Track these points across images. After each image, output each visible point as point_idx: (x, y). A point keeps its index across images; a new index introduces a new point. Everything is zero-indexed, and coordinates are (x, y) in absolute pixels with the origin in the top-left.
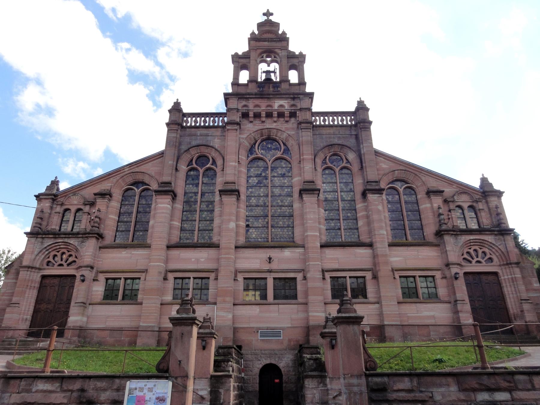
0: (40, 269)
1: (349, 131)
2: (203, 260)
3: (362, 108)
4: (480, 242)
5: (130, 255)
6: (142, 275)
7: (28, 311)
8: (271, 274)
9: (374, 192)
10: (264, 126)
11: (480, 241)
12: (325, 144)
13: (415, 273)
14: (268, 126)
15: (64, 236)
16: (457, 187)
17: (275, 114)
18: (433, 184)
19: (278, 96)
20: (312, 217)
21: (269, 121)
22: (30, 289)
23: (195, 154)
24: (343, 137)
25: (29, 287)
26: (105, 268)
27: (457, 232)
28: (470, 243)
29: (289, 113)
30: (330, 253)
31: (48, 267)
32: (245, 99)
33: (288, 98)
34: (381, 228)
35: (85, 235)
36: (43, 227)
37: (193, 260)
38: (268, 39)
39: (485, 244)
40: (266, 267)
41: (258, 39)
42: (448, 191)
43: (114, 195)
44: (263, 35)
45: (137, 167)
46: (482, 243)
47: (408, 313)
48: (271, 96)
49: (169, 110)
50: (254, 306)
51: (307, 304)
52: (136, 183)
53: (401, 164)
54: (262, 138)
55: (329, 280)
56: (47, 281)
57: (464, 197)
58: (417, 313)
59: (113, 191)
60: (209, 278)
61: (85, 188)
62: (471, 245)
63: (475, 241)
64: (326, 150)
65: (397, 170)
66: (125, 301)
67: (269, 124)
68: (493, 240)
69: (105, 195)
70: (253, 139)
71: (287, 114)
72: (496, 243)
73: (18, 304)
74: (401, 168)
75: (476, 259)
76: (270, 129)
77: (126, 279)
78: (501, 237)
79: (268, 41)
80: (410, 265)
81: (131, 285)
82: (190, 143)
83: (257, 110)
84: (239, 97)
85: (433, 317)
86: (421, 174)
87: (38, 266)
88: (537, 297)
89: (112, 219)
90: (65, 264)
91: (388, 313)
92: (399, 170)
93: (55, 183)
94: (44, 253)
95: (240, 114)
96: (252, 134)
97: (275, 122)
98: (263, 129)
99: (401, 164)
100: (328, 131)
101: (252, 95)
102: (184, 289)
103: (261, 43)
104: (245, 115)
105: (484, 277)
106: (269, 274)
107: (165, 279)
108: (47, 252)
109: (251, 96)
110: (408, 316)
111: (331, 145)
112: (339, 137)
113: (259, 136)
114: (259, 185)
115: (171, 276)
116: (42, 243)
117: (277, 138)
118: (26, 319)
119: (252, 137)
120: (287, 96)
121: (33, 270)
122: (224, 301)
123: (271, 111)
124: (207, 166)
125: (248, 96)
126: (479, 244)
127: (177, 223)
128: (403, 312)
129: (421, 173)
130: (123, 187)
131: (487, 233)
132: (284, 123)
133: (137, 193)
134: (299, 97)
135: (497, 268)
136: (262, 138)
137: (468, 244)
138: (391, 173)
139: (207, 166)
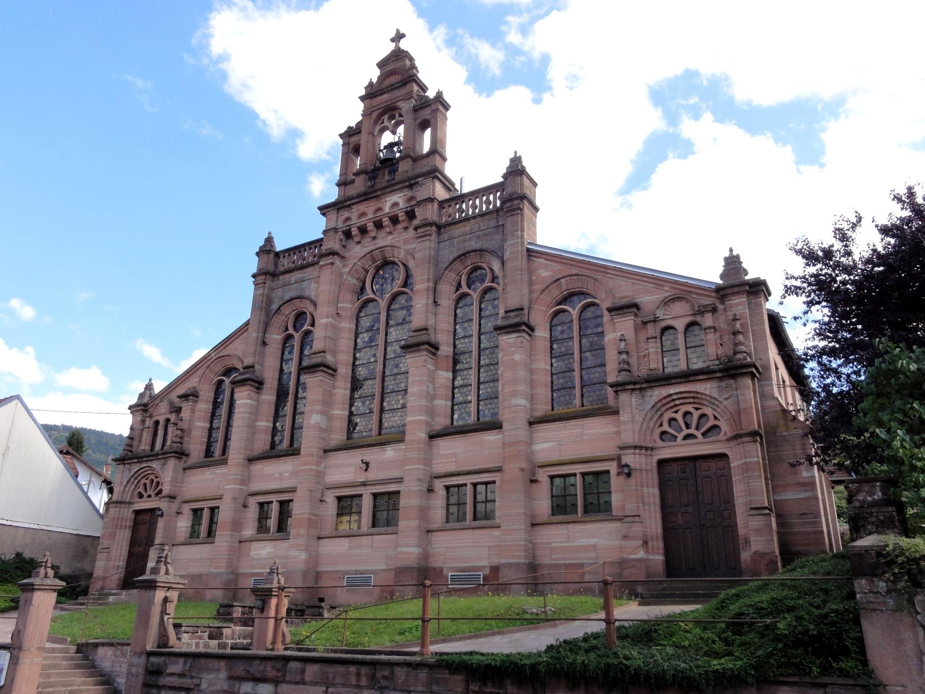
0: (130, 503)
1: (496, 221)
2: (287, 475)
3: (516, 170)
4: (694, 398)
5: (213, 476)
6: (611, 465)
7: (120, 556)
8: (368, 488)
9: (509, 330)
10: (376, 243)
11: (692, 395)
12: (456, 255)
13: (574, 469)
14: (380, 243)
15: (706, 377)
16: (672, 288)
17: (386, 221)
18: (625, 291)
19: (388, 190)
20: (415, 390)
21: (382, 233)
22: (121, 529)
23: (289, 311)
24: (485, 235)
25: (119, 527)
26: (188, 497)
27: (642, 383)
28: (674, 400)
29: (403, 214)
30: (445, 446)
31: (140, 500)
32: (346, 209)
33: (402, 188)
34: (514, 394)
35: (164, 455)
36: (134, 449)
37: (277, 475)
38: (387, 88)
39: (702, 399)
40: (362, 478)
41: (372, 94)
42: (649, 299)
43: (201, 393)
44: (385, 82)
45: (225, 348)
46: (696, 398)
47: (554, 542)
48: (379, 193)
49: (267, 249)
50: (342, 539)
51: (533, 525)
52: (567, 298)
53: (573, 263)
54: (375, 264)
55: (442, 492)
56: (141, 517)
57: (680, 308)
58: (567, 542)
59: (199, 388)
60: (361, 495)
61: (174, 389)
62: (676, 405)
63: (685, 397)
64: (458, 266)
65: (564, 277)
66: (452, 525)
67: (384, 240)
68: (716, 390)
69: (191, 396)
70: (362, 271)
71: (402, 216)
72: (720, 396)
73: (639, 516)
74: (574, 271)
75: (686, 432)
76: (381, 247)
77: (475, 485)
78: (732, 382)
79: (388, 91)
80: (566, 457)
81: (484, 494)
82: (282, 298)
83: (363, 221)
84: (338, 207)
85: (594, 547)
86: (608, 276)
87: (128, 500)
88: (805, 499)
89: (198, 427)
90: (698, 434)
91: (508, 543)
92: (573, 275)
93: (149, 387)
94: (133, 482)
95: (340, 235)
96: (359, 263)
97: (390, 233)
98: (372, 251)
99: (573, 263)
100: (463, 230)
101: (353, 198)
102: (568, 495)
103: (379, 98)
104: (348, 234)
105: (703, 465)
106: (363, 488)
107: (430, 490)
108: (136, 481)
109: (353, 202)
110: (552, 548)
111: (464, 254)
112: (479, 237)
113: (370, 263)
114: (369, 345)
115: (439, 485)
116: (130, 469)
117: (396, 260)
118: (118, 566)
119: (359, 268)
120: (400, 186)
121: (123, 505)
122: (298, 535)
123: (379, 218)
124: (304, 329)
125: (349, 203)
126: (692, 400)
127: (265, 424)
128: (545, 541)
129: (607, 273)
130: (213, 379)
131: (701, 377)
132: (403, 232)
133: (574, 317)
134: (418, 182)
135: (726, 445)
136: (375, 264)
137: (669, 402)
138: (554, 285)
139: (304, 329)
